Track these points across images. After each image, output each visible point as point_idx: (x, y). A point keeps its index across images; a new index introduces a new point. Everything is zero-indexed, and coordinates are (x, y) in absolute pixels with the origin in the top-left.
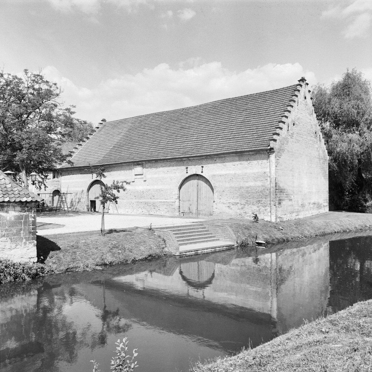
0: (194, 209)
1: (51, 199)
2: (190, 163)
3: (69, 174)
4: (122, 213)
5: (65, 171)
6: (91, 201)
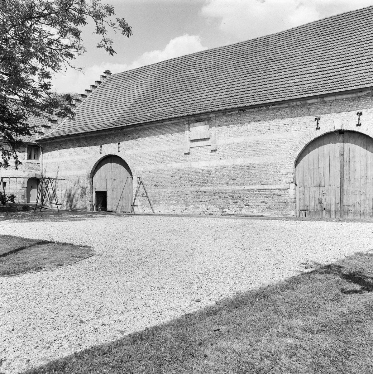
0: (332, 201)
1: (24, 191)
2: (326, 108)
3: (56, 148)
4: (162, 212)
5: (49, 144)
6: (96, 192)
